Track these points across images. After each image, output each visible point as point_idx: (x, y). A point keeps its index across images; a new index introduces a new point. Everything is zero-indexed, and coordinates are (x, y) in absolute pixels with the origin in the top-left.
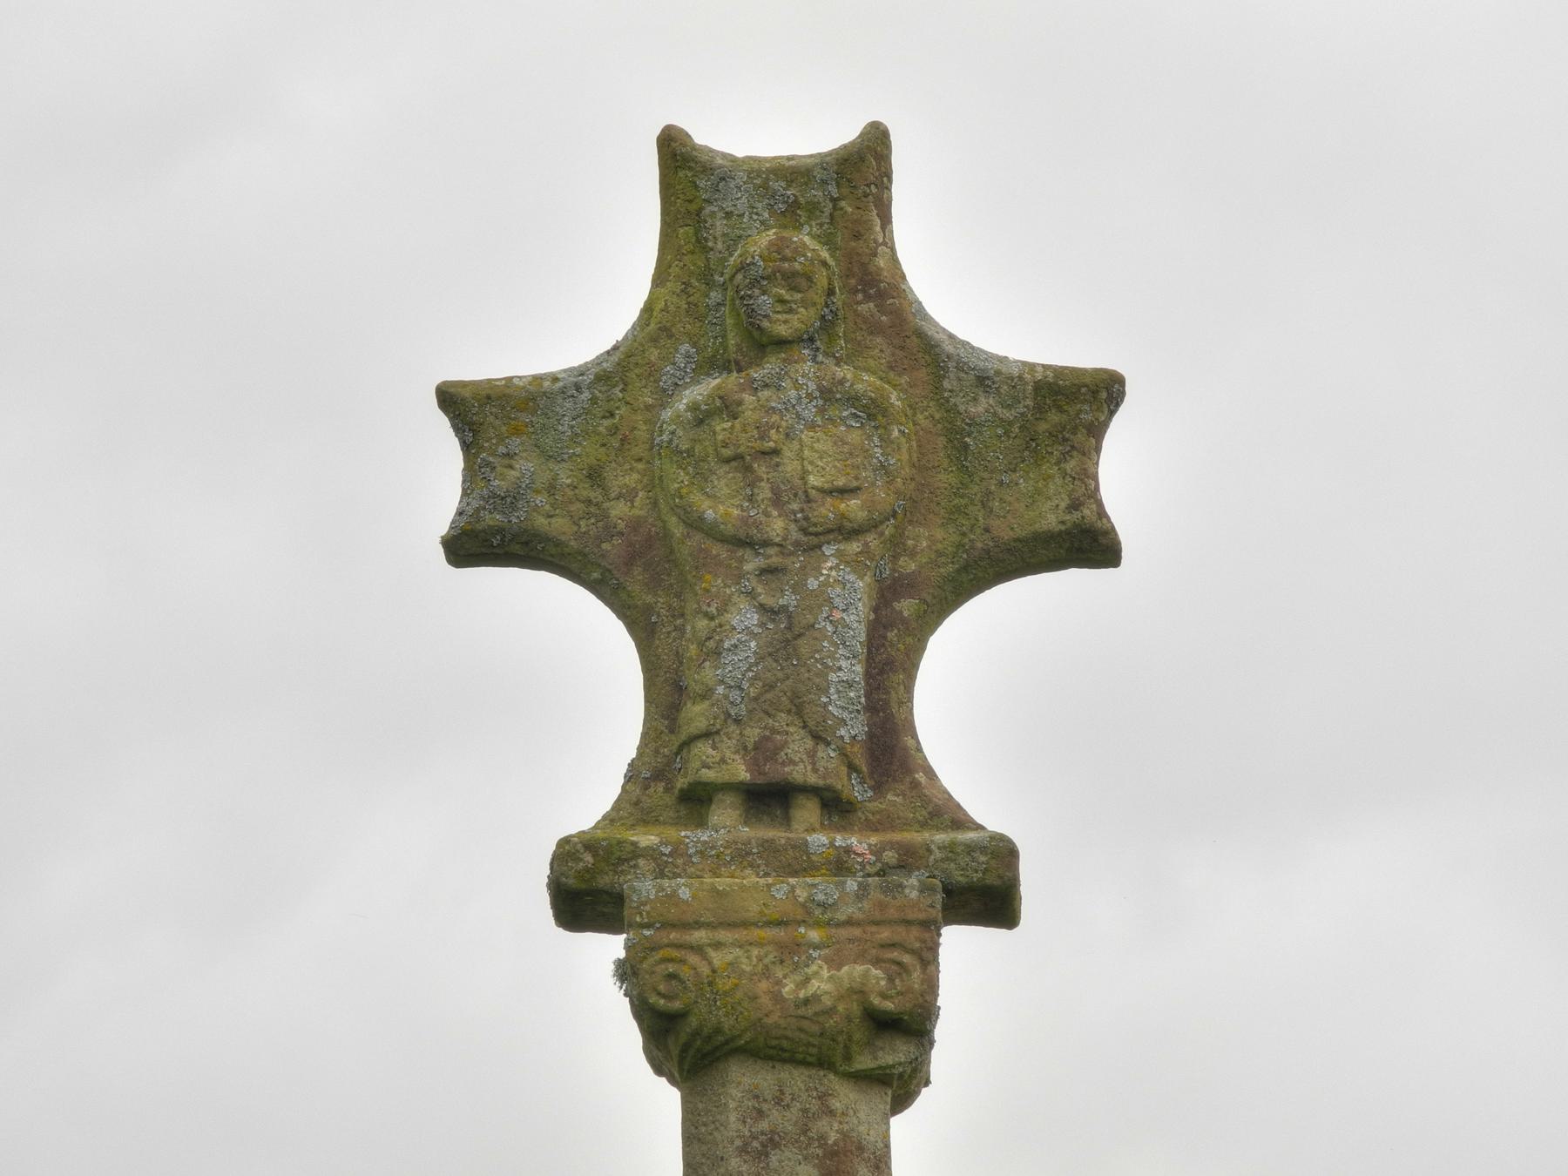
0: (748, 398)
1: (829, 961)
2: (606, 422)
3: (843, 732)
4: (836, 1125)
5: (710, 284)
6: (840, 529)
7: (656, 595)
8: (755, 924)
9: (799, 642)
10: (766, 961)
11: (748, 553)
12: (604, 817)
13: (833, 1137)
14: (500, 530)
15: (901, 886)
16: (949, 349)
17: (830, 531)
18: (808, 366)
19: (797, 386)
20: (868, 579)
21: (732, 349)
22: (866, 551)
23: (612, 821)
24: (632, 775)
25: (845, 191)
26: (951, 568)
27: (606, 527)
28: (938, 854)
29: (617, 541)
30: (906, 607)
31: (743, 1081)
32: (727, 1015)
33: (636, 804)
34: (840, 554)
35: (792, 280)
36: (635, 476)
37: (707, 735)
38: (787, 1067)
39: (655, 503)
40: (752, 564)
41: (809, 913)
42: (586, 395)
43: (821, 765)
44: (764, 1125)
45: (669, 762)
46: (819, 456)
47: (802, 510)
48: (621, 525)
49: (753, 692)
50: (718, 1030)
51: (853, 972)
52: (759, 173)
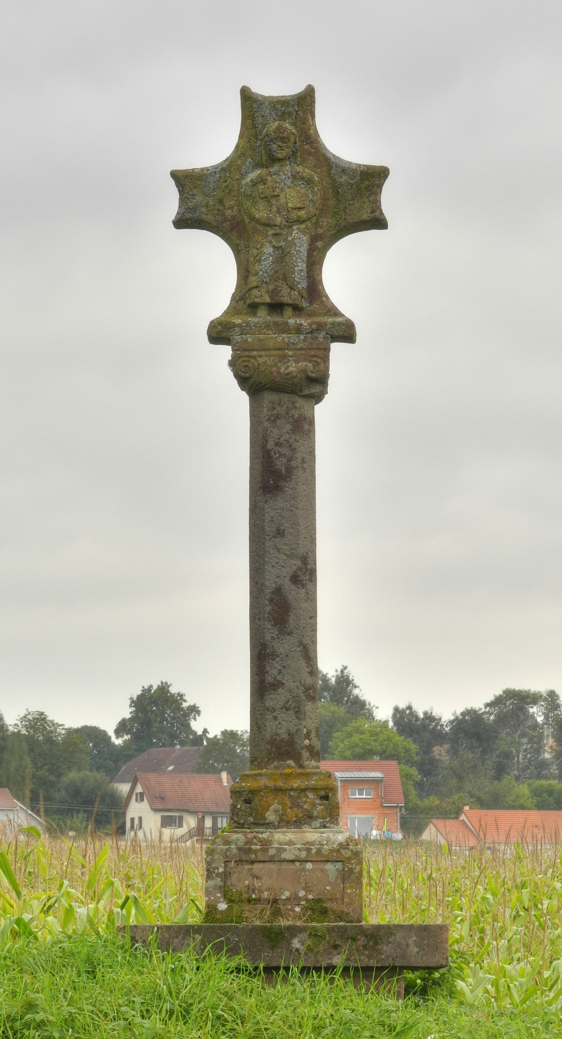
0: (269, 178)
1: (295, 361)
2: (224, 184)
3: (299, 286)
4: (297, 412)
5: (257, 139)
6: (298, 221)
7: (240, 241)
8: (272, 350)
9: (286, 257)
10: (275, 361)
11: (269, 228)
12: (225, 312)
13: (296, 416)
14: (190, 219)
15: (317, 337)
16: (333, 160)
17: (295, 221)
18: (288, 167)
19: (285, 174)
20: (307, 236)
21: (264, 161)
22: (307, 228)
23: (227, 313)
24: (233, 298)
25: (300, 108)
26: (334, 232)
27: (224, 218)
28: (329, 326)
29: (228, 223)
30: (320, 244)
31: (268, 397)
32: (263, 378)
33: (235, 308)
34: (298, 229)
35: (283, 140)
36: (234, 202)
37: (257, 287)
38: (282, 393)
39: (240, 211)
40: (271, 232)
41: (288, 346)
42: (218, 175)
43: (292, 297)
44: (275, 412)
45: (245, 294)
46: (291, 197)
47: (286, 215)
48: (229, 218)
49: (271, 274)
50: (260, 383)
51: (303, 364)
52: (273, 102)
